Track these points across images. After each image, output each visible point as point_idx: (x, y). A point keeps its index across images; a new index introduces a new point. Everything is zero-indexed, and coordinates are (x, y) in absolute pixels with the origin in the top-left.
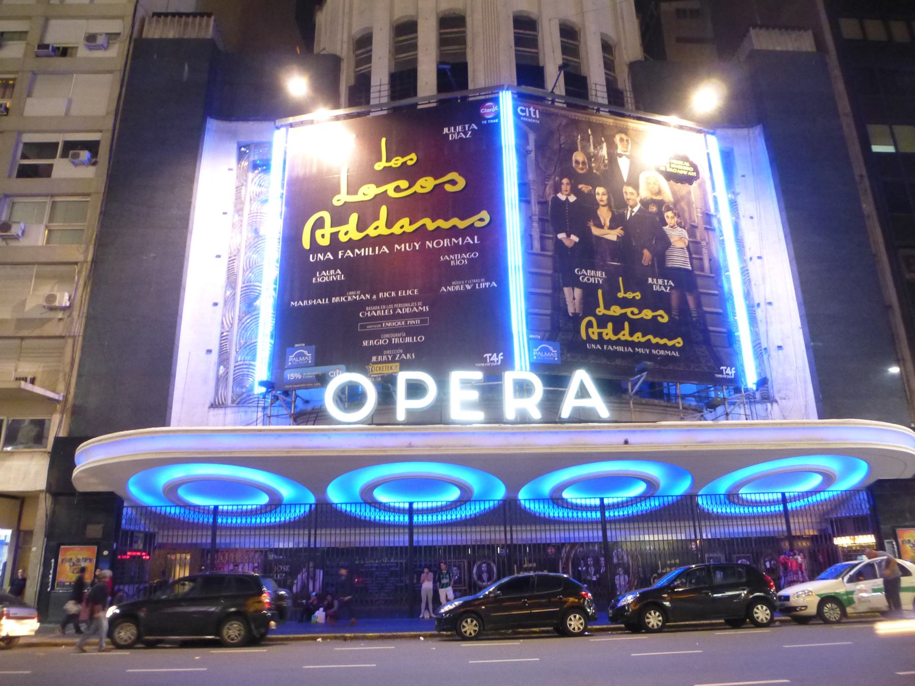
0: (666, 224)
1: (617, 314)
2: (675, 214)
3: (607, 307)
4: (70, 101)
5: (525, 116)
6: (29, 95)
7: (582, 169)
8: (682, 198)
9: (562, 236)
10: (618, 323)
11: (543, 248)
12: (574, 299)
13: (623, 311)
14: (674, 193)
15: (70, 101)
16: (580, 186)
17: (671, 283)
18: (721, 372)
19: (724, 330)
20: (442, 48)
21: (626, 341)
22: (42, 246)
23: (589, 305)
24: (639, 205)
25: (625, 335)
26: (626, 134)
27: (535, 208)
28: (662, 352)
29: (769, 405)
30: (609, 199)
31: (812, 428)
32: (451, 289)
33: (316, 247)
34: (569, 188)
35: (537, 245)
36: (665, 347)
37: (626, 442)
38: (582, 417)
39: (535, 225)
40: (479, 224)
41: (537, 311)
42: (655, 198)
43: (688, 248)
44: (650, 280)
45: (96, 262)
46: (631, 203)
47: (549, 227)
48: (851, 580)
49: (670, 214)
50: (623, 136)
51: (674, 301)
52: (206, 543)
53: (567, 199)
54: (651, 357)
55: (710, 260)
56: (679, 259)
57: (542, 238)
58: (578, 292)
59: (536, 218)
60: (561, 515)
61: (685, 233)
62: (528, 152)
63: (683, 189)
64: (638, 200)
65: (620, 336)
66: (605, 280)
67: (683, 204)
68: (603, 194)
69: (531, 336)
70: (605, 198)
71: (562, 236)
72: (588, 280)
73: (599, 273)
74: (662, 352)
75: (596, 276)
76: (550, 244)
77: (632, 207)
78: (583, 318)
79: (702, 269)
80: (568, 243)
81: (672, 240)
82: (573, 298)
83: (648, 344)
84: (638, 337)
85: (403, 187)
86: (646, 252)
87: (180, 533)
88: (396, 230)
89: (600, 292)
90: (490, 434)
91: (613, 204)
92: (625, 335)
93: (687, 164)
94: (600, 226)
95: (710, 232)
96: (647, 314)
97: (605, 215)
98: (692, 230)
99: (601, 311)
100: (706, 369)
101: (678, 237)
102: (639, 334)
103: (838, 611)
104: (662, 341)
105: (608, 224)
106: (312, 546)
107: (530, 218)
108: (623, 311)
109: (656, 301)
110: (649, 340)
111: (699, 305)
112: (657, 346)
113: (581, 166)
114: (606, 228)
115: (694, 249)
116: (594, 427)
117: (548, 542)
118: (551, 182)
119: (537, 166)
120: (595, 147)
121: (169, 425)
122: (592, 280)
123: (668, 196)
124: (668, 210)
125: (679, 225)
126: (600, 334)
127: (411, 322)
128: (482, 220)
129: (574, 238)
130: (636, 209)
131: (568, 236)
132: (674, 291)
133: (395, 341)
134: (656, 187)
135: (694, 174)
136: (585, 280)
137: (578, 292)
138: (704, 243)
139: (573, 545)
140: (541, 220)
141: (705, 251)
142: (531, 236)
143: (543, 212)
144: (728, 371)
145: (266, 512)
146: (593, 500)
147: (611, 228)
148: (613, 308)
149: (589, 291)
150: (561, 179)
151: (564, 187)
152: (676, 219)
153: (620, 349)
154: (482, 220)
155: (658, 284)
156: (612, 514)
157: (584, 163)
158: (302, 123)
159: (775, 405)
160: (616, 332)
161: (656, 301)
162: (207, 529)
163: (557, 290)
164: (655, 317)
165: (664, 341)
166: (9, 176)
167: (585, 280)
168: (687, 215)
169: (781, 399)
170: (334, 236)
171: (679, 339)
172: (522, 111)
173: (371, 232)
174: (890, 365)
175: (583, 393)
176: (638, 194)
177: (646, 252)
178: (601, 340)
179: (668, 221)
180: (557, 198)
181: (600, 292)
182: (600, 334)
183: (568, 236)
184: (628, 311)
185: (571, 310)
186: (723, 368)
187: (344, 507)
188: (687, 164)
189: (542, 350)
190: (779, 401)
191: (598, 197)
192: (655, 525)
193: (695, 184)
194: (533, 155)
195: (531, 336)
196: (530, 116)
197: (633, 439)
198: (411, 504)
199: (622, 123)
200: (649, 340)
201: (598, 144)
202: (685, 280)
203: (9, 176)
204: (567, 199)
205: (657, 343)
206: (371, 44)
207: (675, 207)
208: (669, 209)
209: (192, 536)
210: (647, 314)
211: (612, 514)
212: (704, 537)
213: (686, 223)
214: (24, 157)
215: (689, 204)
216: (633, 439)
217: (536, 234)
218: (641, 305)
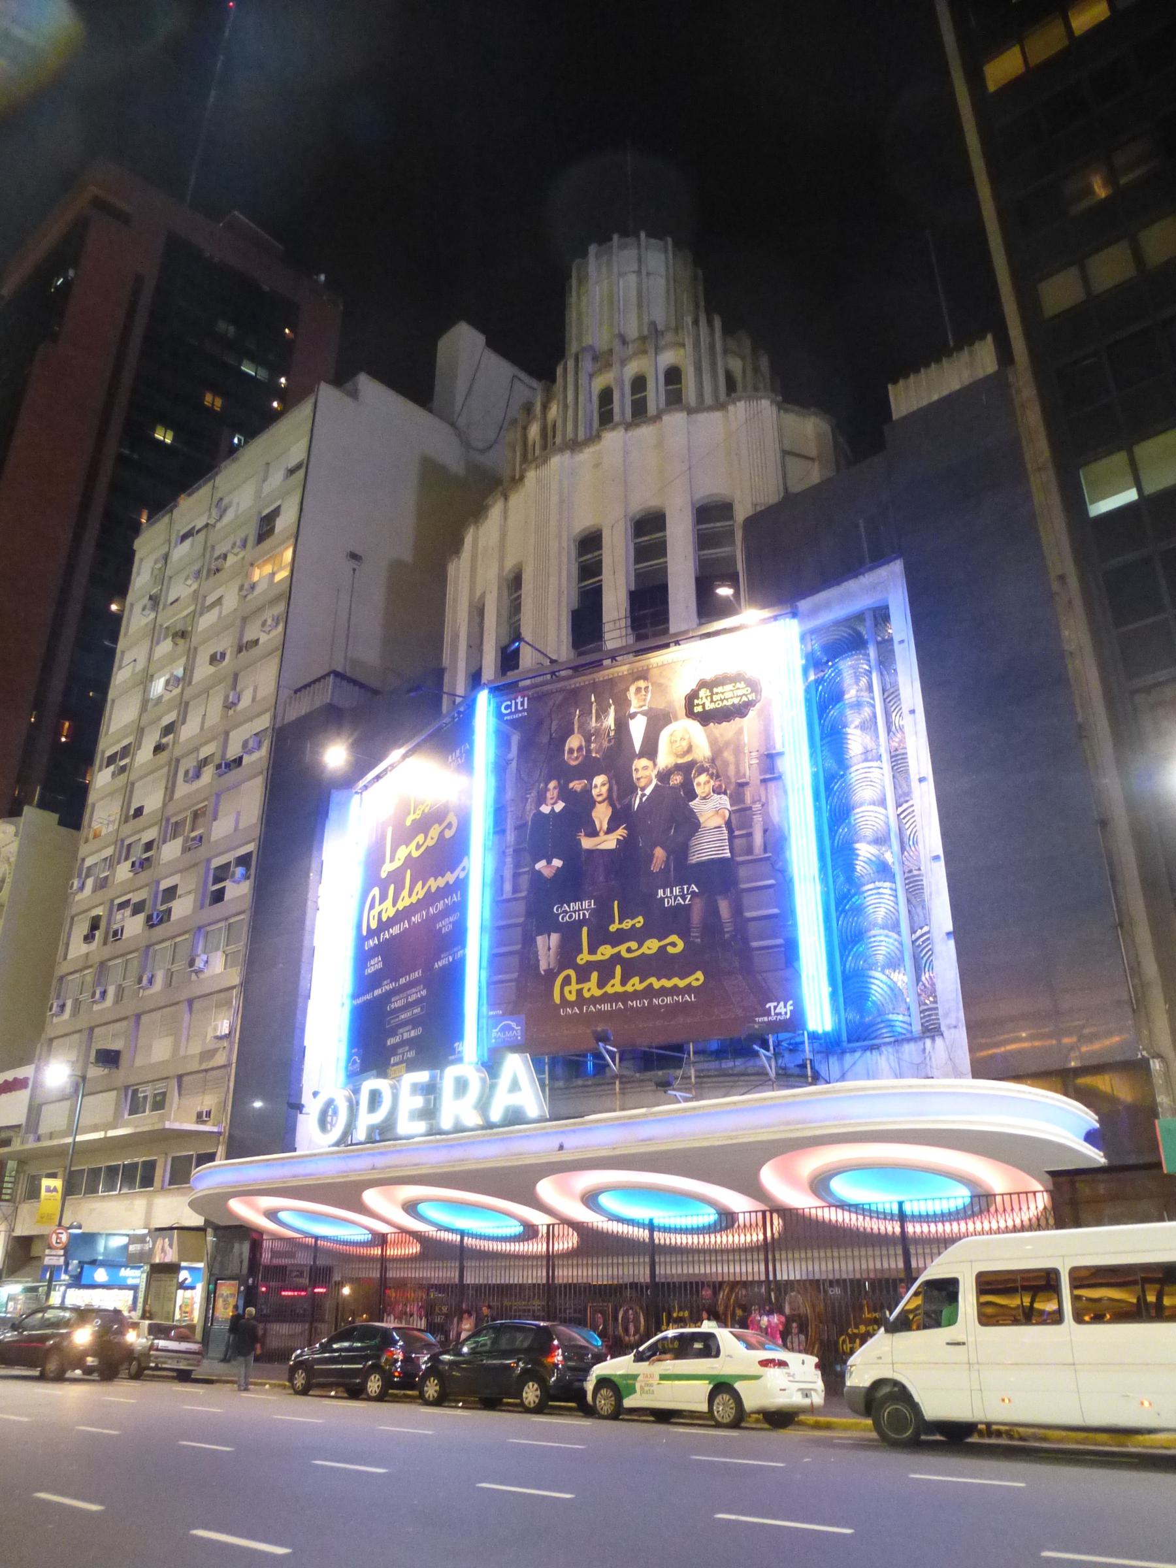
0: (693, 796)
1: (607, 957)
2: (711, 776)
3: (592, 951)
4: (238, 814)
5: (511, 713)
6: (215, 819)
7: (577, 758)
8: (727, 744)
9: (540, 865)
10: (605, 970)
11: (515, 890)
12: (549, 949)
13: (616, 950)
14: (713, 742)
15: (238, 814)
16: (571, 785)
17: (694, 888)
18: (767, 1013)
19: (780, 941)
20: (701, 527)
21: (616, 993)
22: (221, 973)
23: (567, 955)
24: (655, 782)
25: (615, 986)
26: (645, 678)
27: (511, 837)
28: (669, 1000)
29: (928, 1042)
30: (610, 790)
31: (781, 1105)
32: (440, 964)
33: (565, 1002)
34: (556, 792)
35: (508, 887)
36: (675, 990)
37: (561, 1147)
38: (515, 1117)
39: (509, 860)
40: (695, 984)
41: (500, 977)
42: (680, 761)
43: (728, 824)
44: (660, 893)
45: (246, 984)
46: (642, 783)
47: (527, 857)
48: (640, 1358)
49: (703, 778)
50: (642, 684)
51: (696, 916)
52: (897, 1269)
53: (553, 810)
54: (651, 1010)
55: (765, 831)
56: (710, 845)
57: (516, 876)
58: (555, 938)
59: (510, 851)
60: (690, 1242)
61: (725, 800)
62: (508, 762)
63: (725, 730)
64: (654, 774)
65: (609, 989)
66: (594, 913)
67: (728, 755)
68: (603, 785)
69: (491, 1013)
70: (604, 789)
71: (540, 865)
72: (570, 917)
73: (586, 904)
74: (669, 1000)
75: (582, 909)
76: (524, 881)
77: (643, 789)
78: (559, 973)
79: (749, 850)
80: (548, 873)
81: (701, 820)
82: (547, 946)
83: (649, 992)
84: (635, 984)
85: (447, 831)
86: (659, 853)
87: (849, 1253)
88: (629, 988)
89: (585, 930)
90: (557, 1133)
91: (615, 795)
92: (615, 986)
93: (742, 685)
94: (594, 833)
95: (772, 785)
96: (652, 946)
97: (601, 815)
98: (737, 792)
99: (584, 958)
100: (740, 1013)
101: (711, 810)
102: (636, 980)
103: (612, 1401)
104: (668, 984)
105: (605, 826)
106: (771, 1278)
107: (504, 852)
108: (616, 950)
109: (676, 920)
110: (651, 984)
111: (737, 911)
112: (664, 992)
113: (575, 754)
114: (602, 833)
115: (738, 824)
116: (520, 1131)
117: (738, 1279)
118: (534, 794)
119: (519, 778)
120: (598, 718)
121: (295, 1150)
122: (575, 916)
123: (703, 751)
124: (700, 774)
125: (717, 791)
126: (579, 992)
127: (417, 1010)
128: (697, 979)
129: (557, 863)
130: (648, 791)
131: (549, 862)
132: (697, 900)
133: (406, 1036)
134: (685, 744)
135: (752, 697)
136: (567, 918)
137: (555, 938)
138: (757, 806)
139: (734, 1285)
140: (517, 851)
141: (758, 819)
142: (502, 877)
143: (519, 840)
144: (781, 1009)
145: (981, 1212)
146: (689, 1218)
147: (609, 831)
148: (602, 949)
149: (570, 933)
150: (547, 785)
151: (549, 795)
152: (712, 783)
153: (606, 1007)
154: (697, 979)
155: (671, 896)
156: (918, 1230)
157: (580, 749)
158: (385, 771)
159: (939, 1040)
160: (601, 984)
161: (676, 920)
162: (895, 1245)
163: (529, 942)
164: (662, 949)
165: (676, 981)
166: (202, 907)
167: (567, 918)
168: (731, 771)
169: (949, 1027)
170: (579, 992)
171: (699, 975)
172: (507, 707)
173: (609, 989)
174: (260, 1109)
175: (515, 1086)
176: (655, 765)
177: (659, 853)
178: (581, 999)
179: (698, 790)
180: (540, 812)
181: (585, 930)
182: (580, 992)
183: (549, 862)
184: (622, 949)
185: (543, 966)
186: (771, 1005)
187: (813, 1211)
188: (742, 685)
189: (503, 1030)
190: (946, 1034)
191: (595, 792)
192: (863, 1253)
193: (752, 713)
194: (514, 764)
195: (491, 1013)
196: (517, 711)
197: (571, 1141)
198: (901, 1204)
199: (643, 663)
200: (651, 984)
201: (602, 712)
202: (719, 878)
203: (202, 907)
204: (553, 810)
205: (663, 988)
206: (665, 555)
207: (714, 767)
208: (702, 770)
209: (860, 1257)
210: (652, 946)
211: (918, 1230)
212: (779, 1278)
213: (728, 784)
214: (214, 883)
215: (738, 751)
216: (571, 1141)
217: (508, 874)
218: (640, 936)
